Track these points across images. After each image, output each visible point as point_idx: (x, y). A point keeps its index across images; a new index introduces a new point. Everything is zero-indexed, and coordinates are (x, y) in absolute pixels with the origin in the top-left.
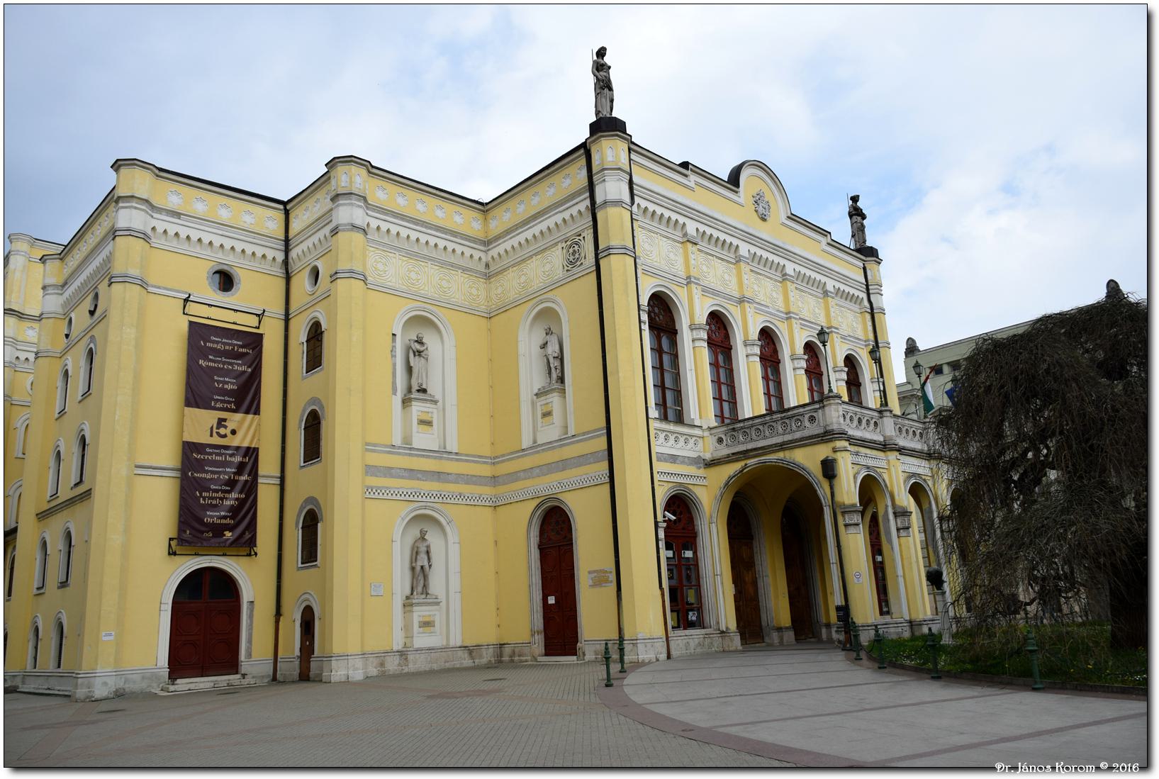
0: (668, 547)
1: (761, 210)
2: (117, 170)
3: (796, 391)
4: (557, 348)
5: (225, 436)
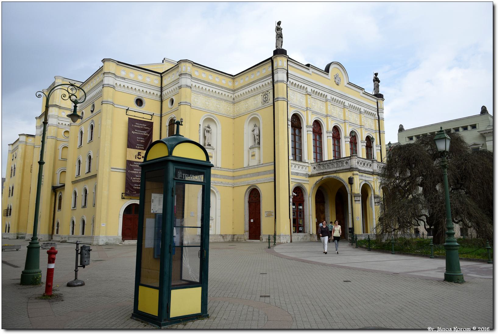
0: (293, 205)
2: (103, 62)
3: (346, 151)
4: (258, 132)
5: (140, 158)
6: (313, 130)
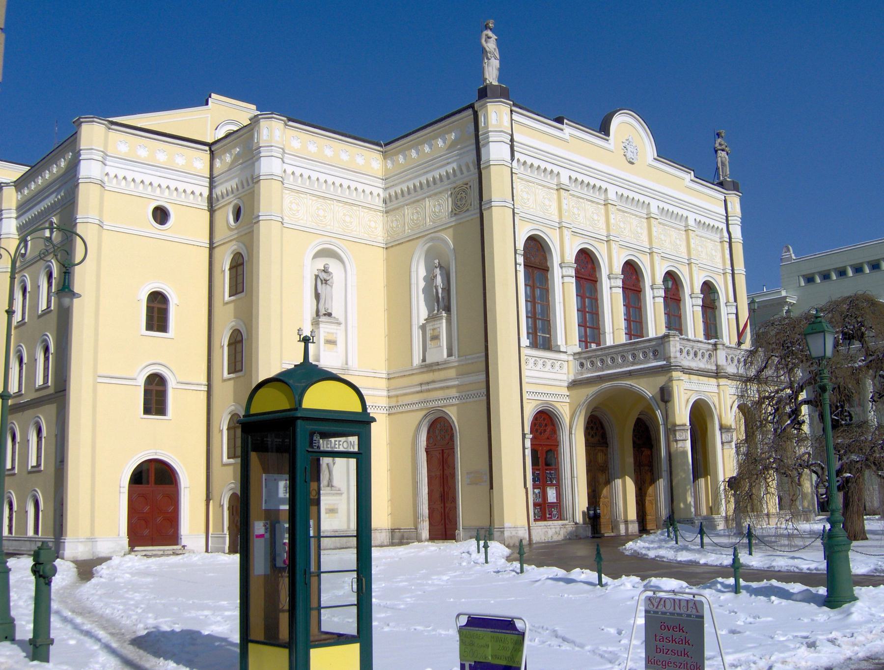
1: (629, 155)
3: (655, 323)
6: (577, 271)
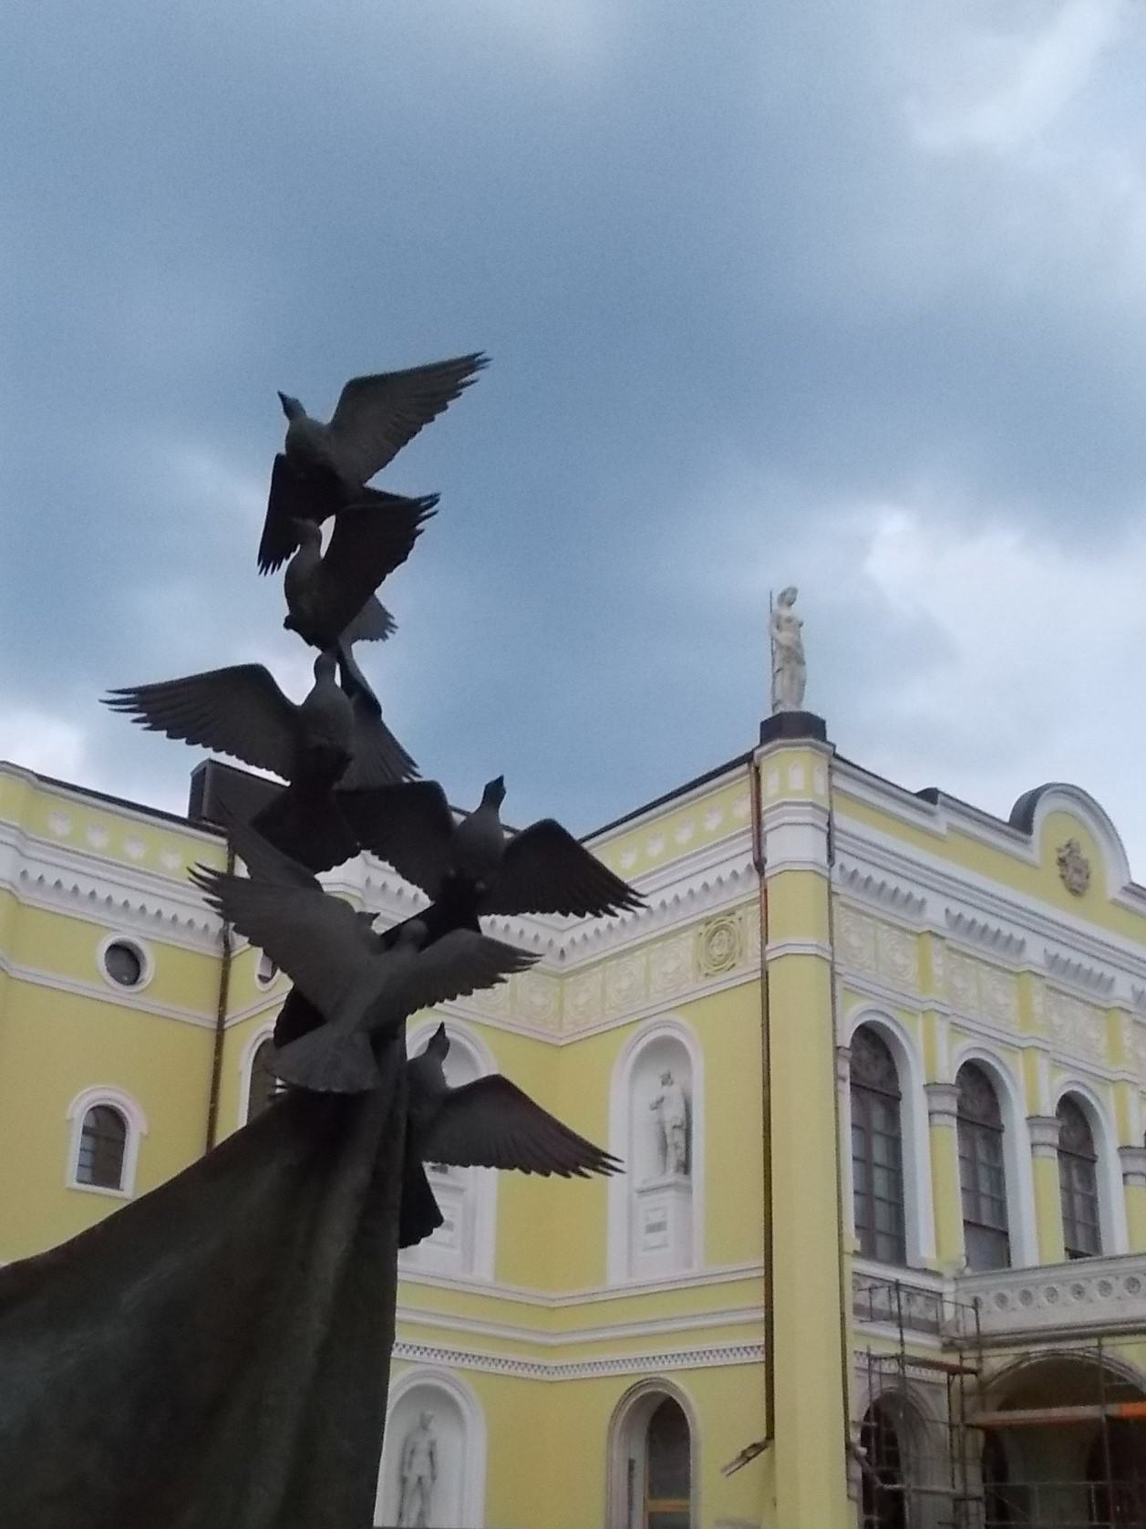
4: (681, 1114)
